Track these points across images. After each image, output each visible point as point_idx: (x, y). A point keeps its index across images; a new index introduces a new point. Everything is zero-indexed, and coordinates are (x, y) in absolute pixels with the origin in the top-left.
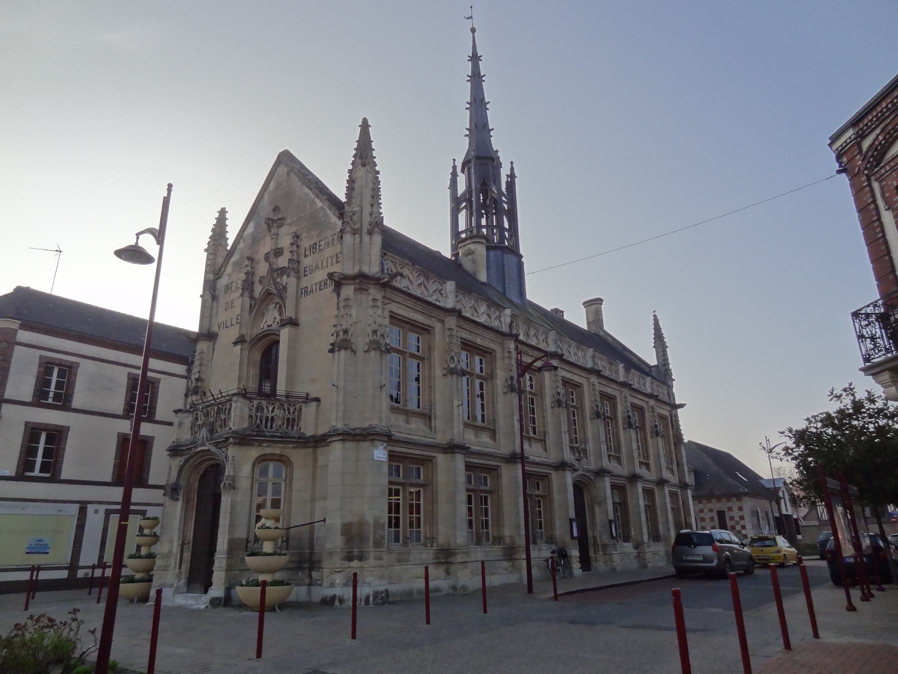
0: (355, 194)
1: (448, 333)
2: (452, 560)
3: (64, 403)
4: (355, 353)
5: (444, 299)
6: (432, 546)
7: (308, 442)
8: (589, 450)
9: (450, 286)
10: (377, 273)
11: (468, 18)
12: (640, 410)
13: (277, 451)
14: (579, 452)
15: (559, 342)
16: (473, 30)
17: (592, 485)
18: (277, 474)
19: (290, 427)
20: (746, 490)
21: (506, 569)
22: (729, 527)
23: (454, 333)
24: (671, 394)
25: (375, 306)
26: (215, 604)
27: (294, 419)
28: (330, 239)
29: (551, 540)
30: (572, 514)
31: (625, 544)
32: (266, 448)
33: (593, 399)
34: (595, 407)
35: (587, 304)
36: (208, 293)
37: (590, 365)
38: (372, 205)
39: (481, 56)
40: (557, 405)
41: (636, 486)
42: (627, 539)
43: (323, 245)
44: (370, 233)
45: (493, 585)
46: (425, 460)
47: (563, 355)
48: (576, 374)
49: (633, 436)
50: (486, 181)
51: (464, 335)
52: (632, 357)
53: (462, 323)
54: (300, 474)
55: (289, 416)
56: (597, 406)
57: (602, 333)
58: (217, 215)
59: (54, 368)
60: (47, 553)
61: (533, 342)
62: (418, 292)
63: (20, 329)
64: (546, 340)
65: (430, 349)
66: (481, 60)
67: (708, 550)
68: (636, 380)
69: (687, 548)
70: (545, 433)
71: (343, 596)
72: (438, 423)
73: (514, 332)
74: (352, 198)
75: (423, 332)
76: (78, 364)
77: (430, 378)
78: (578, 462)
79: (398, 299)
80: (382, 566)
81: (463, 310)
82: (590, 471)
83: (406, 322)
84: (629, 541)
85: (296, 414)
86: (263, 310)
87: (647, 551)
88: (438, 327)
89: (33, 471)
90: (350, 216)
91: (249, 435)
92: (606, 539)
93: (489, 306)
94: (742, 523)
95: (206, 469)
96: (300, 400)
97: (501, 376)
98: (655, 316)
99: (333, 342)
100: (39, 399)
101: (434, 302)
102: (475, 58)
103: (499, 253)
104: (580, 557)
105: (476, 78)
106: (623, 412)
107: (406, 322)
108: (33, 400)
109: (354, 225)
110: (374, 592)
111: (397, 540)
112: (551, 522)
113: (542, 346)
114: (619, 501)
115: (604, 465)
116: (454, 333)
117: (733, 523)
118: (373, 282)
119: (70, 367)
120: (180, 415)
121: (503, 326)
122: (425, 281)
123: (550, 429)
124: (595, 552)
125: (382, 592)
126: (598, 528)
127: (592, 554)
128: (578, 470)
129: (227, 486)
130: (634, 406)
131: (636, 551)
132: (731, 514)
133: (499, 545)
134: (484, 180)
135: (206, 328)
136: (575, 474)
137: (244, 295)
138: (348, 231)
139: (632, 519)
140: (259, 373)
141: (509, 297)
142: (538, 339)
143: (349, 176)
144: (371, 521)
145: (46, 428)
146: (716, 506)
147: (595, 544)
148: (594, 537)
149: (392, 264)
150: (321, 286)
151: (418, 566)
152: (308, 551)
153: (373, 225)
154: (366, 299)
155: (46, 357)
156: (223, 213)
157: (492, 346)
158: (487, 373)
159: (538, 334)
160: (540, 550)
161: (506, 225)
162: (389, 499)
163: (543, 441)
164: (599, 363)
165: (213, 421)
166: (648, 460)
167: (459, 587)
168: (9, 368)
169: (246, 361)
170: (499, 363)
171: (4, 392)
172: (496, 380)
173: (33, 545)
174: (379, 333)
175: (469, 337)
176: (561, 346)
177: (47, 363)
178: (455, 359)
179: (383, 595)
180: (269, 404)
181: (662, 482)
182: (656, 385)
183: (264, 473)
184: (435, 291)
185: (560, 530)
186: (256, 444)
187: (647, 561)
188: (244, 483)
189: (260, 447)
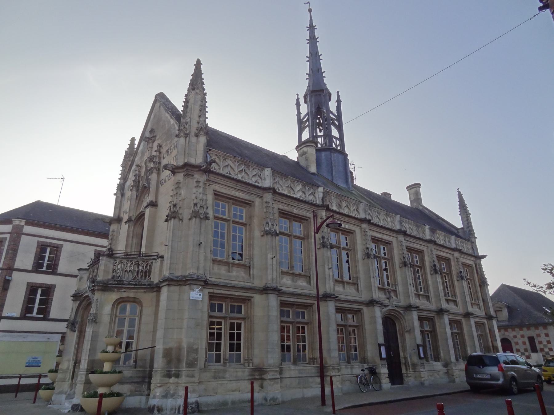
0: (188, 110)
1: (265, 205)
3: (53, 270)
6: (249, 366)
7: (153, 288)
8: (399, 292)
9: (267, 172)
11: (307, 3)
14: (389, 293)
16: (310, 10)
17: (403, 318)
18: (133, 312)
19: (143, 278)
20: (550, 320)
22: (514, 349)
23: (270, 204)
26: (75, 409)
27: (146, 272)
28: (176, 144)
29: (364, 360)
31: (435, 363)
32: (123, 293)
34: (402, 259)
35: (409, 188)
36: (119, 192)
37: (398, 227)
38: (200, 117)
40: (366, 257)
42: (437, 358)
44: (197, 135)
45: (305, 396)
46: (245, 300)
48: (385, 234)
50: (320, 106)
52: (444, 223)
54: (148, 311)
56: (404, 258)
57: (421, 208)
58: (129, 142)
59: (47, 248)
60: (40, 366)
61: (346, 211)
62: (239, 177)
63: (25, 225)
64: (357, 210)
65: (250, 217)
66: (316, 29)
67: (494, 370)
68: (442, 238)
69: (476, 368)
70: (357, 278)
71: (162, 406)
72: (255, 271)
74: (186, 113)
75: (246, 205)
76: (62, 246)
78: (388, 300)
79: (218, 180)
80: (194, 383)
82: (400, 307)
83: (230, 199)
84: (439, 361)
85: (148, 267)
87: (454, 368)
88: (257, 201)
89: (32, 313)
91: (111, 284)
92: (415, 359)
93: (304, 186)
94: (549, 346)
96: (151, 258)
98: (459, 193)
99: (167, 214)
100: (37, 268)
102: (312, 28)
103: (328, 153)
105: (313, 41)
106: (430, 262)
107: (230, 199)
108: (32, 269)
109: (186, 131)
111: (218, 360)
112: (363, 346)
115: (411, 302)
117: (542, 346)
118: (197, 169)
119: (57, 247)
120: (81, 272)
122: (246, 169)
123: (362, 276)
126: (409, 350)
128: (388, 306)
129: (90, 321)
130: (439, 258)
131: (445, 369)
132: (540, 339)
133: (314, 365)
135: (117, 215)
136: (385, 309)
138: (182, 136)
139: (441, 343)
141: (336, 183)
142: (350, 210)
145: (41, 286)
146: (527, 333)
147: (406, 364)
148: (405, 358)
149: (216, 157)
151: (233, 382)
154: (192, 182)
155: (42, 242)
158: (304, 235)
159: (350, 205)
160: (352, 368)
162: (211, 329)
163: (356, 284)
166: (455, 298)
168: (18, 249)
169: (131, 234)
171: (14, 265)
173: (30, 361)
174: (199, 206)
175: (286, 208)
176: (371, 215)
177: (42, 245)
178: (270, 223)
179: (194, 406)
180: (128, 261)
181: (468, 315)
182: (461, 242)
183: (123, 310)
184: (255, 176)
185: (371, 352)
186: (116, 290)
188: (105, 318)
189: (119, 292)
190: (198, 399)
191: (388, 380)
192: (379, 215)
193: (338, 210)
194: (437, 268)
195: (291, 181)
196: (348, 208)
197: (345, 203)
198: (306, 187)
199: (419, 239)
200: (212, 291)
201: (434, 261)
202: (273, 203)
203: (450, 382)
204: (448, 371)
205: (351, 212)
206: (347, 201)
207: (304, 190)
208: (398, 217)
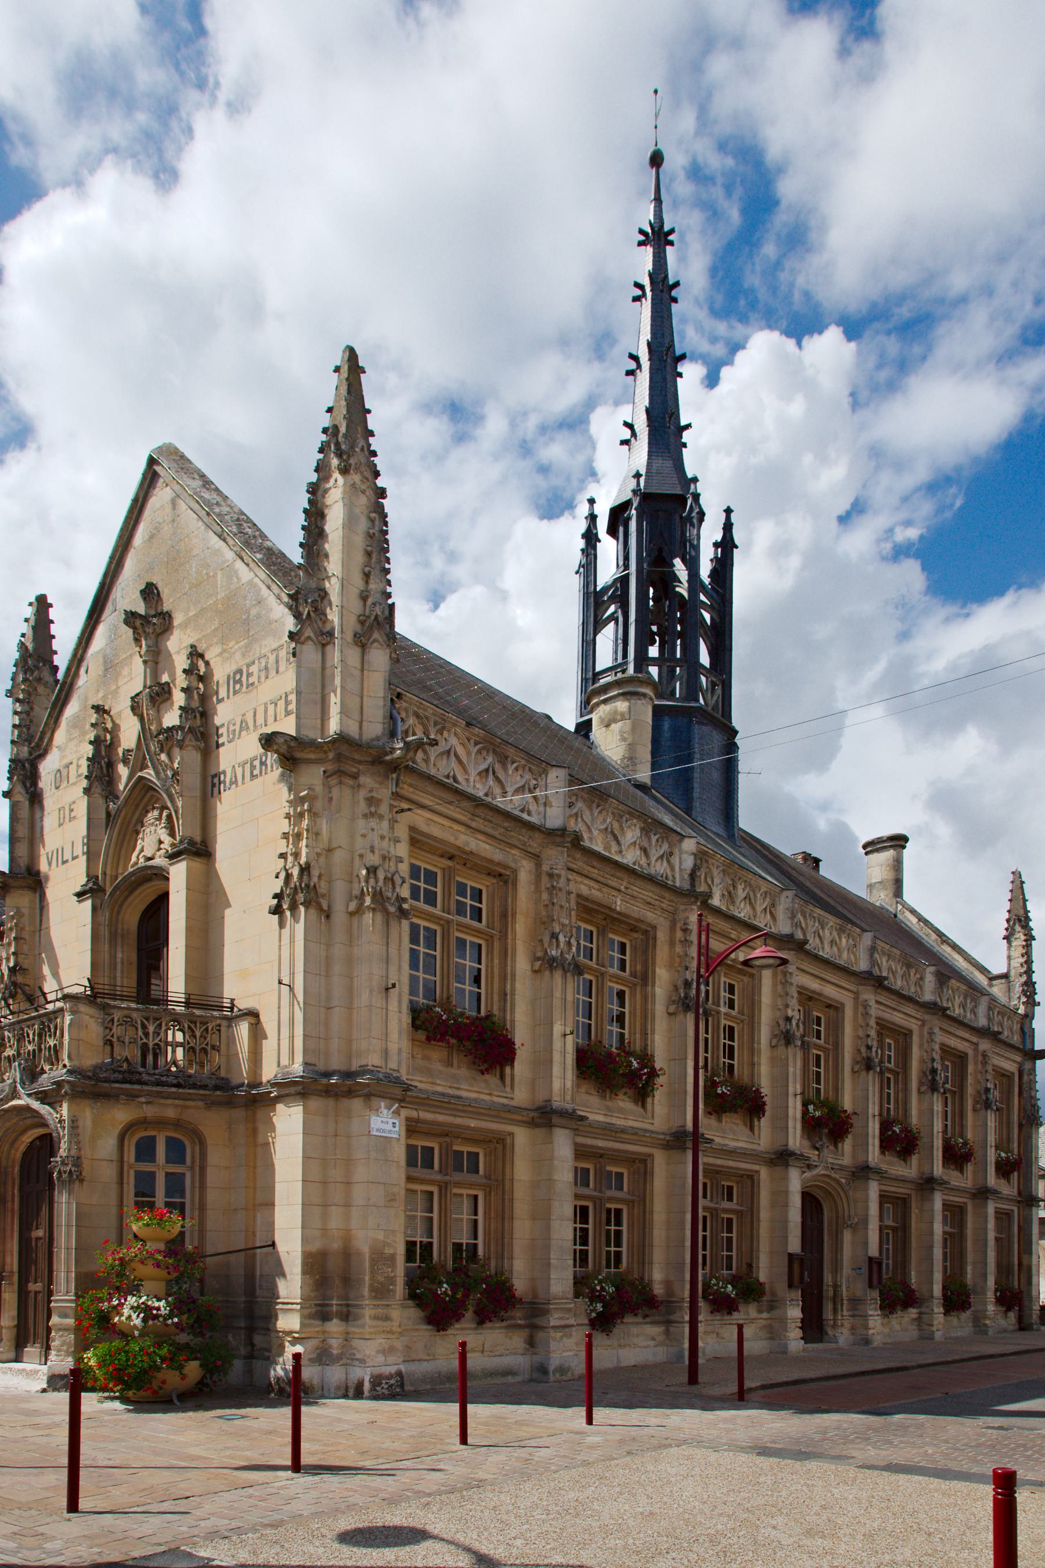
2: (538, 1321)
4: (328, 917)
5: (542, 809)
10: (378, 739)
12: (959, 1060)
13: (171, 1113)
15: (799, 915)
21: (653, 1339)
23: (562, 883)
24: (1026, 1030)
25: (372, 815)
30: (794, 1245)
33: (861, 1033)
34: (863, 1050)
38: (367, 576)
39: (672, 231)
40: (782, 1042)
41: (932, 1200)
43: (256, 674)
47: (805, 942)
48: (833, 984)
49: (938, 1107)
50: (664, 554)
51: (586, 888)
52: (956, 956)
53: (580, 864)
55: (145, 1040)
61: (742, 912)
62: (479, 790)
64: (771, 910)
66: (671, 243)
71: (311, 1380)
73: (702, 888)
77: (503, 978)
78: (817, 1153)
81: (586, 836)
82: (842, 1168)
86: (135, 825)
90: (314, 601)
93: (646, 831)
95: (31, 1143)
97: (663, 977)
99: (278, 891)
101: (517, 812)
104: (803, 1321)
106: (922, 1061)
110: (372, 1376)
113: (762, 921)
114: (893, 1224)
116: (562, 883)
121: (677, 876)
122: (497, 766)
124: (835, 1311)
125: (390, 1376)
126: (846, 1270)
127: (828, 1314)
134: (660, 550)
137: (93, 790)
138: (309, 638)
140: (134, 957)
142: (754, 909)
143: (310, 501)
144: (366, 1250)
148: (836, 1287)
150: (253, 767)
152: (243, 1299)
153: (367, 624)
156: (42, 604)
157: (650, 916)
159: (755, 896)
161: (705, 659)
164: (884, 962)
165: (34, 1050)
167: (551, 1368)
170: (662, 953)
172: (653, 985)
174: (381, 875)
176: (803, 926)
178: (561, 938)
179: (392, 1381)
181: (983, 1193)
182: (999, 1013)
187: (934, 1328)
190: (402, 1367)
191: (799, 1333)
192: (823, 928)
193: (724, 908)
194: (938, 1078)
195: (613, 813)
196: (750, 903)
197: (744, 890)
198: (652, 836)
199: (909, 999)
200: (414, 1114)
201: (933, 1060)
202: (568, 880)
203: (921, 1338)
204: (919, 1317)
205: (755, 916)
206: (751, 885)
207: (645, 844)
208: (867, 939)
